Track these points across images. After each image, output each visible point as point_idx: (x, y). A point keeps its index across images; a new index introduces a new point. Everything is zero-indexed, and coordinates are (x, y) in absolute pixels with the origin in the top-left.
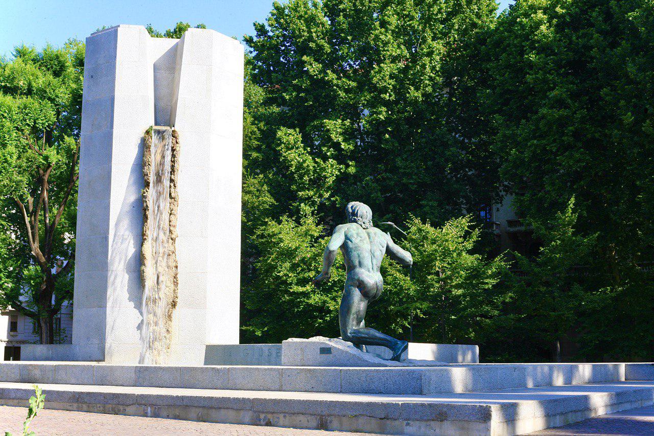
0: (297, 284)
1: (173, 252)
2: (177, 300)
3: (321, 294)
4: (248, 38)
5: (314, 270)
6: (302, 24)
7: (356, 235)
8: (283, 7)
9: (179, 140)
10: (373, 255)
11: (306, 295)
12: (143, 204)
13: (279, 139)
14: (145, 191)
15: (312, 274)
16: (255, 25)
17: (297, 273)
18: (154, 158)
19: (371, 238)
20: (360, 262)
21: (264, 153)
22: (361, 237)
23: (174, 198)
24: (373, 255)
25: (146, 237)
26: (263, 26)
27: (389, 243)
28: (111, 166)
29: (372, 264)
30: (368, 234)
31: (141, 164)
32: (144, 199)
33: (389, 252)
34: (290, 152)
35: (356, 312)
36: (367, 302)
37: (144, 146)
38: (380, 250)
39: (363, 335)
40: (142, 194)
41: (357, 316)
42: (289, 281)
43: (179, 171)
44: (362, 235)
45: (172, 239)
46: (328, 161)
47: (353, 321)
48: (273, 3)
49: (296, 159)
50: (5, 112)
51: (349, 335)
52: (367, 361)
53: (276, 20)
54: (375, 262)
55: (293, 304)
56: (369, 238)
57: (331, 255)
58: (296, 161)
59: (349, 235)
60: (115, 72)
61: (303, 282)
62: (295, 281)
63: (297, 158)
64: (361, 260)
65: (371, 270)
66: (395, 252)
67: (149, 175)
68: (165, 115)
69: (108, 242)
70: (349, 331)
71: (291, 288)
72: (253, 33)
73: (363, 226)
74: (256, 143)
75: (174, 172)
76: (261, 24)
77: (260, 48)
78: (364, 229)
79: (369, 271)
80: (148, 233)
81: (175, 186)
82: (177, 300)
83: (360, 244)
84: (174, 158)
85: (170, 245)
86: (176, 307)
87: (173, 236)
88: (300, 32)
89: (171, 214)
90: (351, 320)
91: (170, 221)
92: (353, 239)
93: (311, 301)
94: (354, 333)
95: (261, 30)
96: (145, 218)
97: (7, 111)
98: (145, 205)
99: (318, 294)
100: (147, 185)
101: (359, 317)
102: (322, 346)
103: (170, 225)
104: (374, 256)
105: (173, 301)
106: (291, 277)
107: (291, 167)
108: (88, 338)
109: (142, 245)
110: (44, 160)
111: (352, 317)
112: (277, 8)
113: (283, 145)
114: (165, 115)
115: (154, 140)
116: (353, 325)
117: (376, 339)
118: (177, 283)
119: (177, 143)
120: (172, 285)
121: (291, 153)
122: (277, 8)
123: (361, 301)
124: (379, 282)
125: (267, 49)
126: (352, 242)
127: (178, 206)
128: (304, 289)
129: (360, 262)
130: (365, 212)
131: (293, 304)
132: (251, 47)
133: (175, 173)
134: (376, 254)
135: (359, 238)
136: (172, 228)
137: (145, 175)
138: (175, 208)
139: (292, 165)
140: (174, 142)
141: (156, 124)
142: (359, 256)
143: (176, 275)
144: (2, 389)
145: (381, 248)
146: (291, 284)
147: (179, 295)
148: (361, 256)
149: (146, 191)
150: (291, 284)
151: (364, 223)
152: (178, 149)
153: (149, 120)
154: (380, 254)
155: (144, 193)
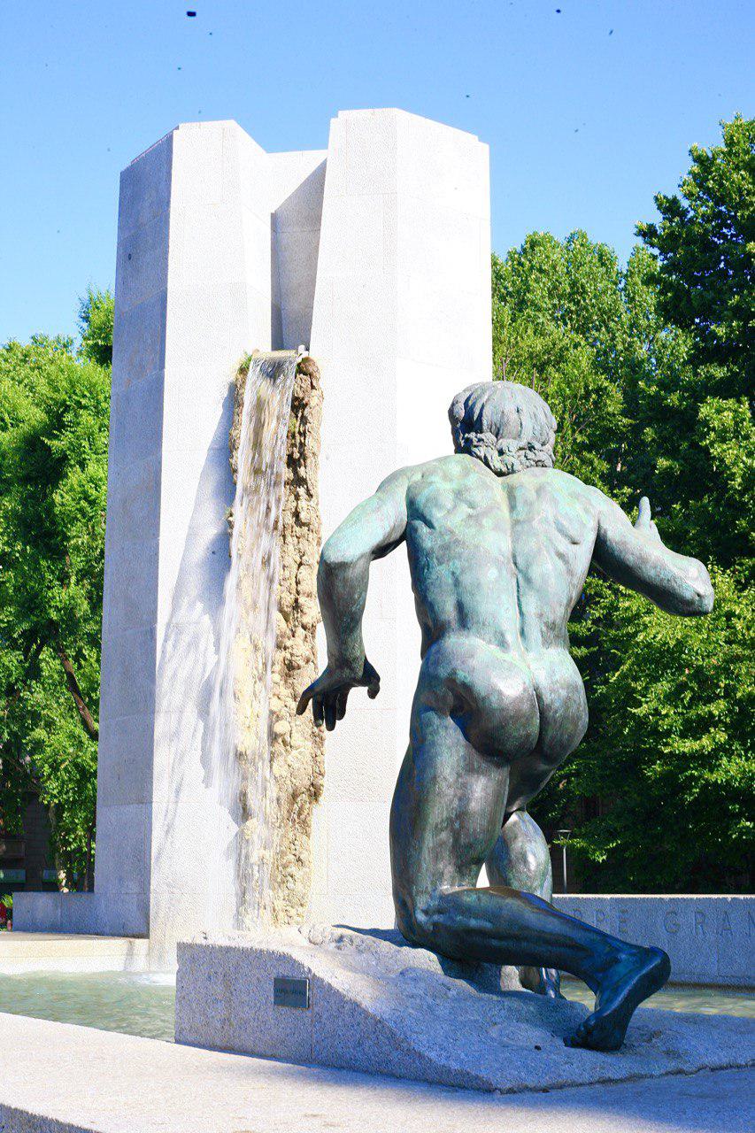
0: (683, 736)
2: (321, 782)
3: (746, 755)
4: (644, 226)
5: (724, 697)
6: (743, 179)
7: (451, 496)
8: (710, 155)
10: (523, 577)
11: (707, 760)
13: (705, 423)
15: (718, 708)
16: (656, 199)
17: (684, 707)
19: (520, 507)
20: (460, 607)
21: (685, 460)
22: (472, 506)
23: (307, 525)
24: (523, 577)
26: (675, 201)
27: (604, 526)
29: (521, 613)
30: (511, 494)
33: (606, 561)
34: (725, 447)
35: (450, 821)
36: (506, 771)
38: (561, 556)
39: (473, 923)
41: (456, 835)
42: (664, 725)
43: (321, 458)
44: (477, 496)
45: (304, 627)
46: (753, 426)
47: (436, 858)
48: (690, 151)
49: (743, 462)
50: (84, 396)
51: (421, 917)
52: (421, 1056)
53: (700, 186)
54: (531, 606)
55: (672, 786)
56: (512, 508)
57: (339, 584)
58: (742, 465)
59: (420, 501)
60: (167, 236)
61: (695, 728)
62: (679, 726)
63: (744, 458)
64: (467, 599)
65: (512, 636)
66: (631, 559)
69: (155, 640)
70: (422, 902)
71: (666, 744)
72: (657, 219)
73: (496, 462)
74: (626, 421)
75: (305, 460)
76: (670, 197)
77: (667, 244)
78: (500, 474)
79: (503, 644)
81: (311, 496)
82: (320, 781)
83: (466, 533)
84: (305, 424)
86: (321, 799)
88: (741, 196)
89: (300, 564)
90: (426, 856)
91: (298, 583)
92: (437, 516)
93: (718, 777)
94: (440, 911)
95: (670, 208)
97: (86, 393)
99: (740, 756)
101: (463, 840)
102: (284, 971)
103: (298, 593)
104: (528, 580)
105: (312, 784)
106: (667, 715)
107: (734, 480)
108: (121, 879)
111: (429, 840)
112: (699, 160)
113: (712, 434)
116: (439, 876)
117: (526, 939)
119: (313, 387)
120: (309, 744)
121: (729, 449)
122: (699, 160)
123: (470, 769)
124: (552, 691)
125: (683, 243)
126: (429, 524)
128: (696, 745)
129: (460, 607)
130: (509, 408)
131: (672, 786)
132: (652, 245)
133: (308, 461)
134: (535, 573)
135: (464, 509)
139: (734, 474)
142: (457, 583)
145: (564, 545)
146: (668, 733)
147: (326, 768)
148: (466, 579)
150: (668, 733)
151: (501, 453)
154: (562, 575)
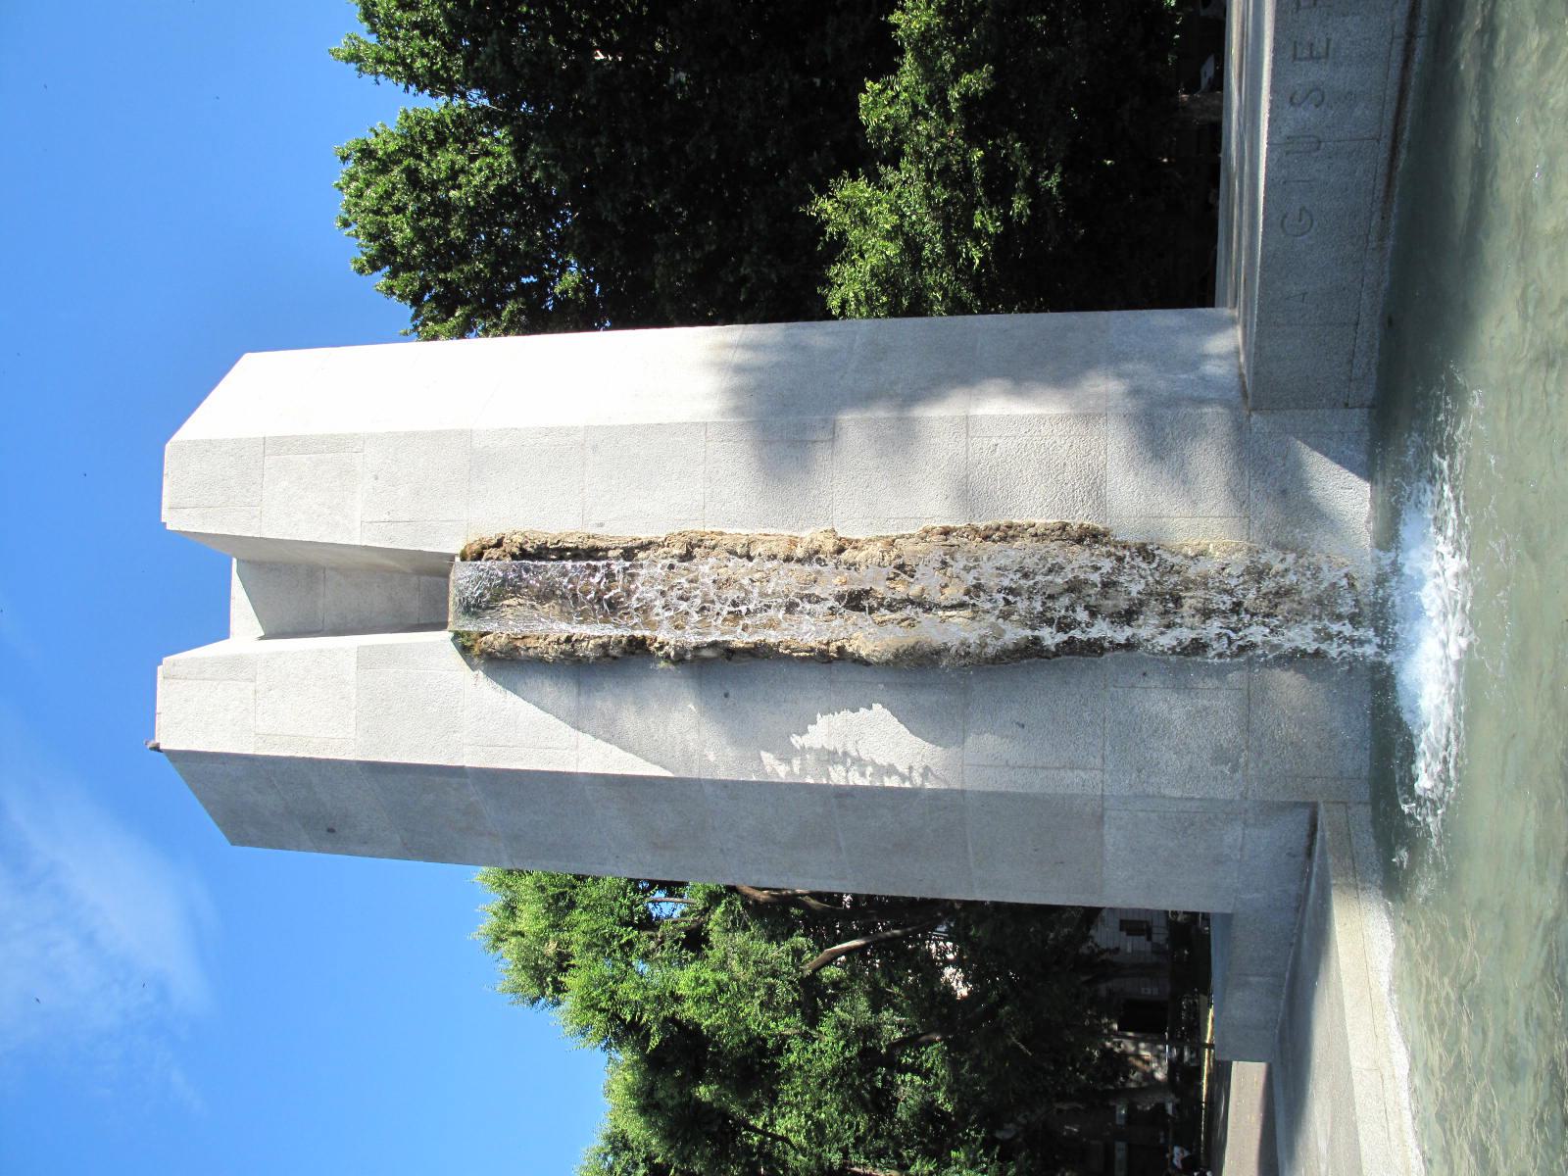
1: (892, 543)
9: (491, 536)
12: (706, 660)
14: (660, 653)
18: (549, 628)
25: (833, 647)
28: (586, 775)
31: (576, 667)
32: (689, 656)
37: (506, 663)
40: (674, 663)
45: (841, 550)
67: (605, 640)
68: (405, 592)
80: (812, 641)
85: (860, 556)
87: (829, 546)
96: (759, 653)
98: (706, 653)
100: (637, 648)
103: (788, 559)
109: (861, 662)
110: (719, 904)
114: (405, 592)
115: (499, 629)
118: (1009, 527)
119: (499, 544)
127: (721, 534)
136: (799, 552)
137: (606, 655)
138: (728, 542)
140: (495, 553)
141: (441, 625)
143: (976, 531)
144: (1208, 33)
149: (661, 648)
152: (519, 539)
153: (433, 651)
155: (667, 656)
